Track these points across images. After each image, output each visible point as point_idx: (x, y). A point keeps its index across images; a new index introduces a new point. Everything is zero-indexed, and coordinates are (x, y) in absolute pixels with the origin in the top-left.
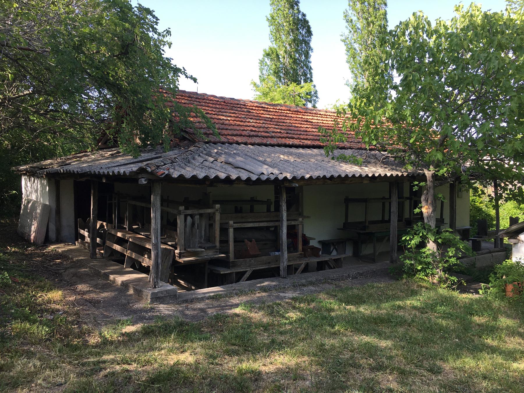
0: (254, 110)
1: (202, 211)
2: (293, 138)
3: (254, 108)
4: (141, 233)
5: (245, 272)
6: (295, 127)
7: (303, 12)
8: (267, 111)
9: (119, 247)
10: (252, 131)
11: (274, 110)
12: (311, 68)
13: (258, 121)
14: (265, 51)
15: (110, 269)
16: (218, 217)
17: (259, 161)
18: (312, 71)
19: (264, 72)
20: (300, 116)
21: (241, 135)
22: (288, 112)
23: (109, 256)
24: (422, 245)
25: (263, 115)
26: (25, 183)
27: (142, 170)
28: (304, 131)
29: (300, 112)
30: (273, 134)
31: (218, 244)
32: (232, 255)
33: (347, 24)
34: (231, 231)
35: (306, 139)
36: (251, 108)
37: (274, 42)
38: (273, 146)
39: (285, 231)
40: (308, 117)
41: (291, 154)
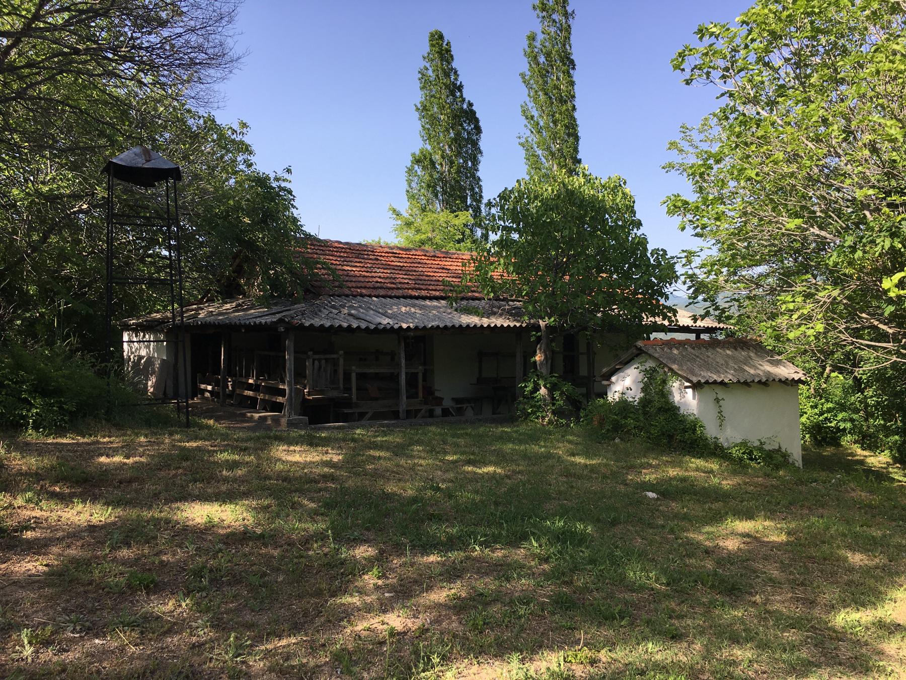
0: (383, 257)
1: (328, 356)
2: (420, 289)
3: (383, 254)
5: (367, 413)
6: (427, 276)
7: (469, 101)
8: (398, 257)
10: (377, 282)
11: (407, 256)
12: (479, 178)
13: (385, 271)
14: (413, 155)
16: (341, 361)
17: (379, 313)
18: (481, 183)
19: (414, 185)
20: (437, 263)
21: (365, 288)
22: (423, 257)
24: (536, 389)
25: (393, 263)
27: (281, 321)
28: (435, 281)
29: (438, 257)
30: (399, 286)
31: (341, 386)
32: (354, 397)
33: (525, 122)
34: (354, 376)
35: (435, 290)
36: (380, 254)
37: (427, 142)
38: (398, 297)
39: (403, 377)
40: (447, 263)
41: (414, 306)
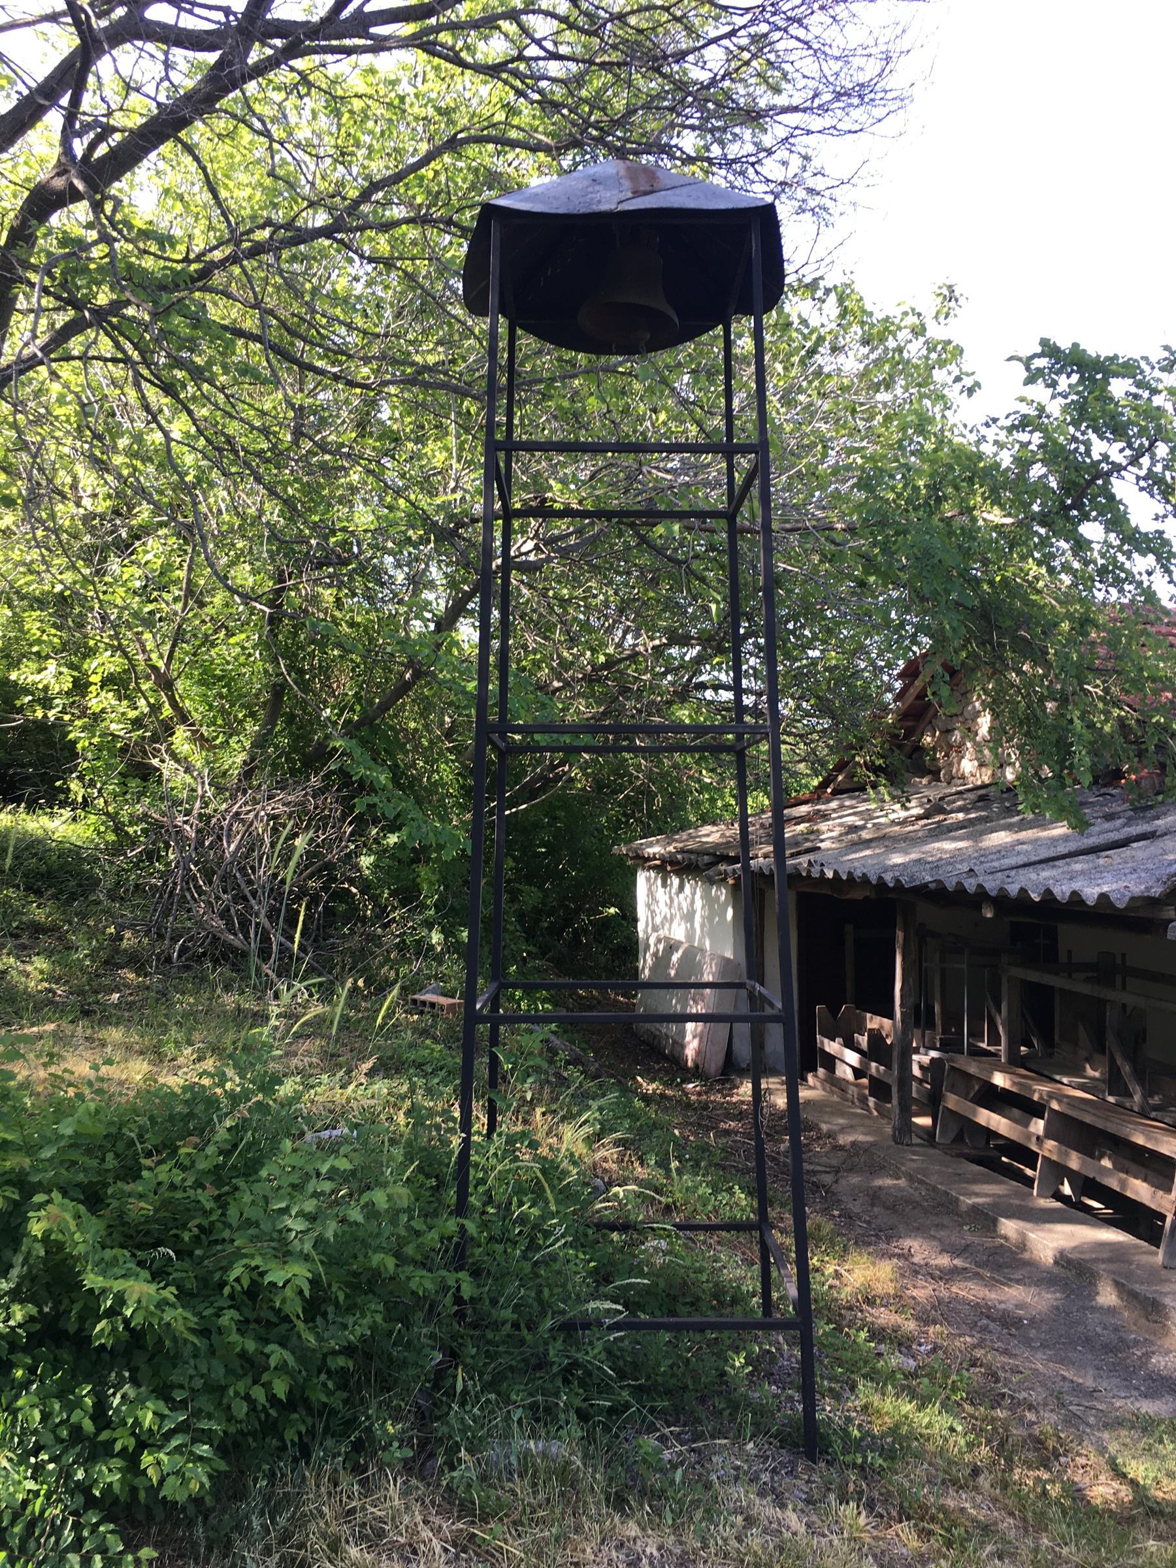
4: (1058, 1077)
9: (1004, 1120)
15: (986, 1195)
23: (954, 1141)
26: (650, 889)
